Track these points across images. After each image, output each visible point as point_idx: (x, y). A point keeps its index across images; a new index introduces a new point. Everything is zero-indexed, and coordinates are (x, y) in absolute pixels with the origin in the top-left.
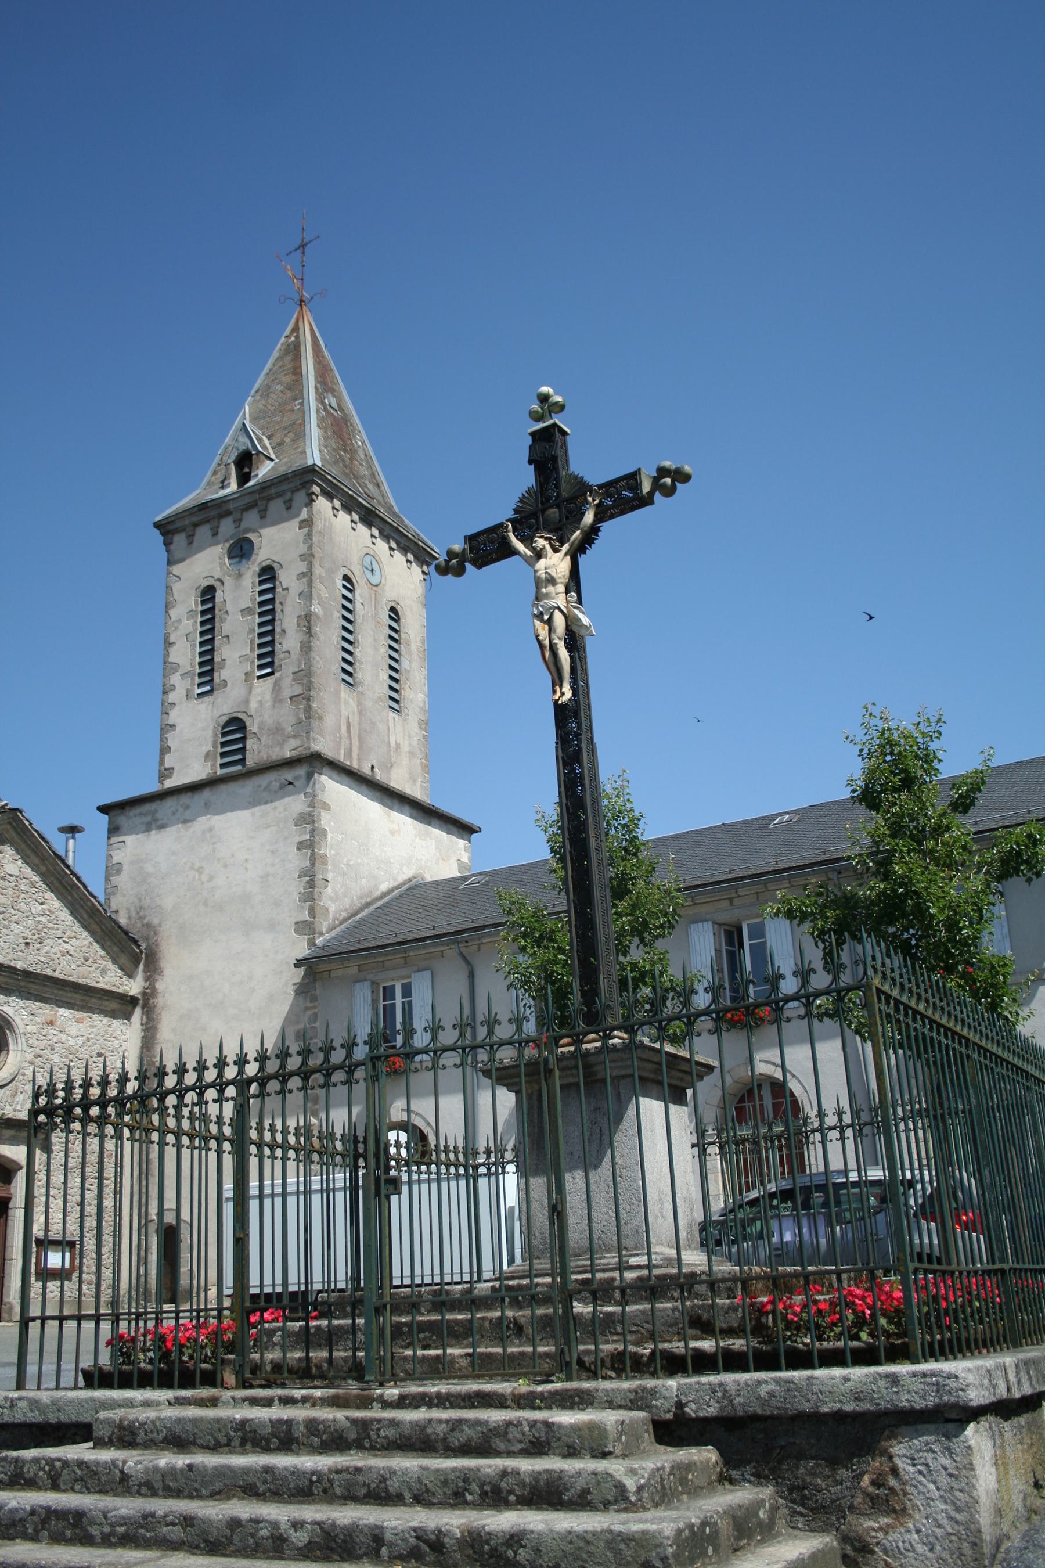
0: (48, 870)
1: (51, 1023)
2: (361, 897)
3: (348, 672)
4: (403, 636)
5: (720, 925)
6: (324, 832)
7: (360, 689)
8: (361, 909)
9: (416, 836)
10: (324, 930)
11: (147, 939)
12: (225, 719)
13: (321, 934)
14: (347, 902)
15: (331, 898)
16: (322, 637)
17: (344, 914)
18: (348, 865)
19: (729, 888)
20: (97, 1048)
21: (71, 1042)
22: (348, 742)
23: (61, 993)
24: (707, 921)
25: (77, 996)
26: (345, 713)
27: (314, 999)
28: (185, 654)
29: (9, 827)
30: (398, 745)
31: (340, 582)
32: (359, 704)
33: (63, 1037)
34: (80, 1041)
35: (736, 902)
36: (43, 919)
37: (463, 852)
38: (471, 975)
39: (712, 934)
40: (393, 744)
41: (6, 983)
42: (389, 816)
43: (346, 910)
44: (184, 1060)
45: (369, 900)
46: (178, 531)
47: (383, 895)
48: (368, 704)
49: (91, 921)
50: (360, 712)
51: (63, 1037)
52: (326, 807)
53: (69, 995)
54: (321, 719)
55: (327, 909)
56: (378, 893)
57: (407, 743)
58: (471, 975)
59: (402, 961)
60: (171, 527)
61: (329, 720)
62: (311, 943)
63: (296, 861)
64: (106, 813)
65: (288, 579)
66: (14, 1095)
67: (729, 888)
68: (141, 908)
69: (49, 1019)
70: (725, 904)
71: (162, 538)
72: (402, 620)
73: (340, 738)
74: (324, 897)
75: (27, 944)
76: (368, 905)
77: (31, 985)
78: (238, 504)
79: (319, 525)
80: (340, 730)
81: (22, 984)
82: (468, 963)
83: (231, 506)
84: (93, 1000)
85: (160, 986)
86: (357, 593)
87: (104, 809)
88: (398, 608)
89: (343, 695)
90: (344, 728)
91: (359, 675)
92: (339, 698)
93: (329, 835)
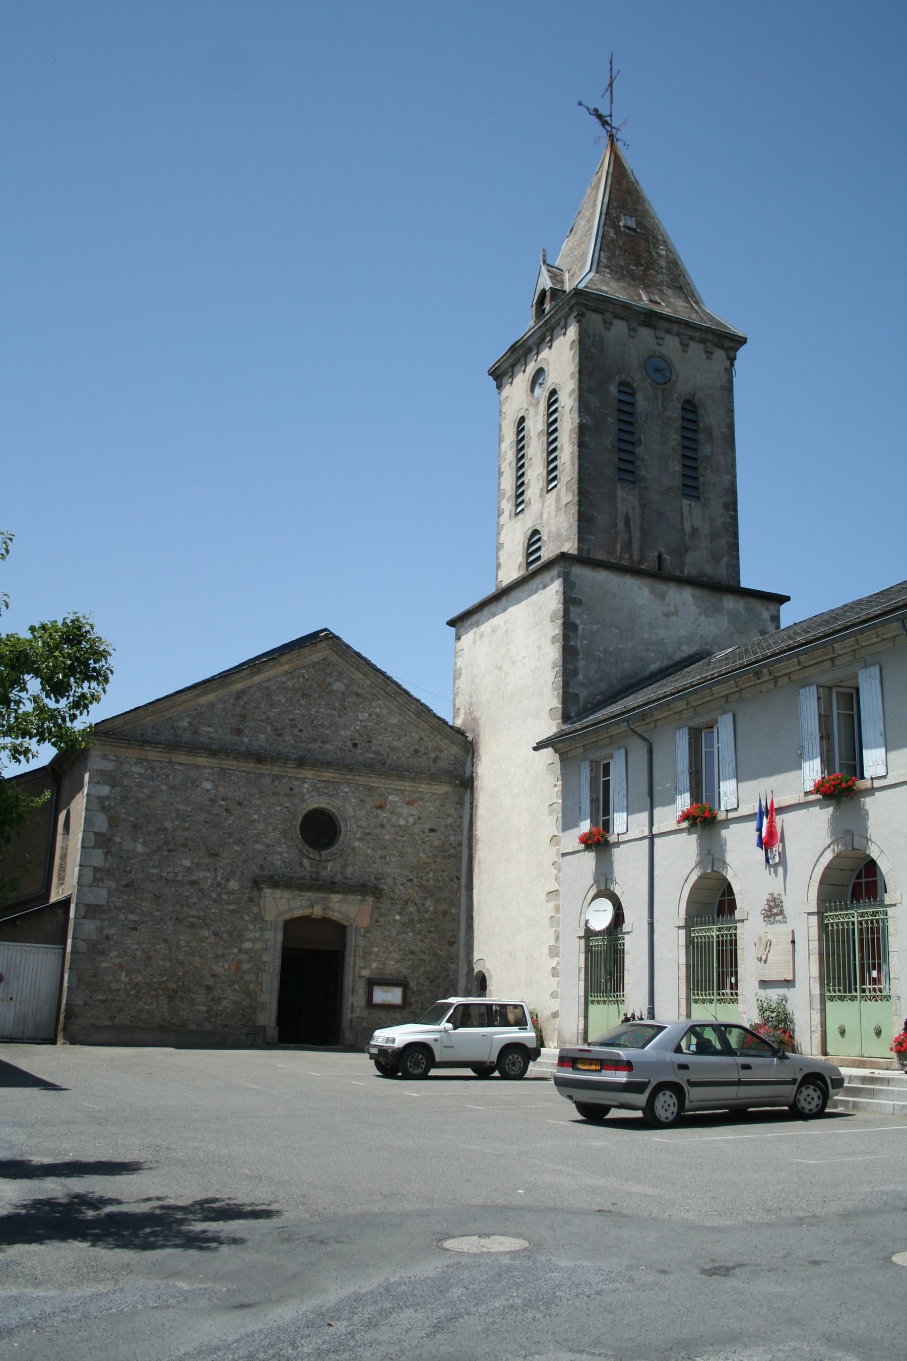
0: (372, 682)
1: (381, 807)
5: (830, 688)
7: (643, 484)
9: (700, 615)
10: (572, 715)
11: (473, 731)
12: (530, 532)
17: (599, 697)
18: (605, 651)
19: (824, 645)
23: (388, 782)
24: (812, 685)
25: (405, 783)
28: (508, 483)
29: (331, 651)
30: (695, 531)
35: (837, 662)
37: (769, 623)
38: (650, 751)
39: (816, 698)
41: (333, 778)
43: (602, 693)
45: (633, 681)
46: (501, 374)
49: (419, 720)
50: (643, 506)
53: (397, 783)
55: (577, 695)
58: (650, 751)
59: (608, 740)
60: (498, 372)
64: (454, 626)
67: (824, 645)
68: (471, 704)
69: (378, 803)
70: (828, 664)
71: (495, 383)
73: (616, 533)
75: (355, 745)
77: (357, 778)
78: (533, 340)
80: (615, 524)
81: (348, 777)
82: (645, 740)
83: (530, 343)
84: (422, 785)
87: (452, 623)
89: (619, 493)
90: (621, 525)
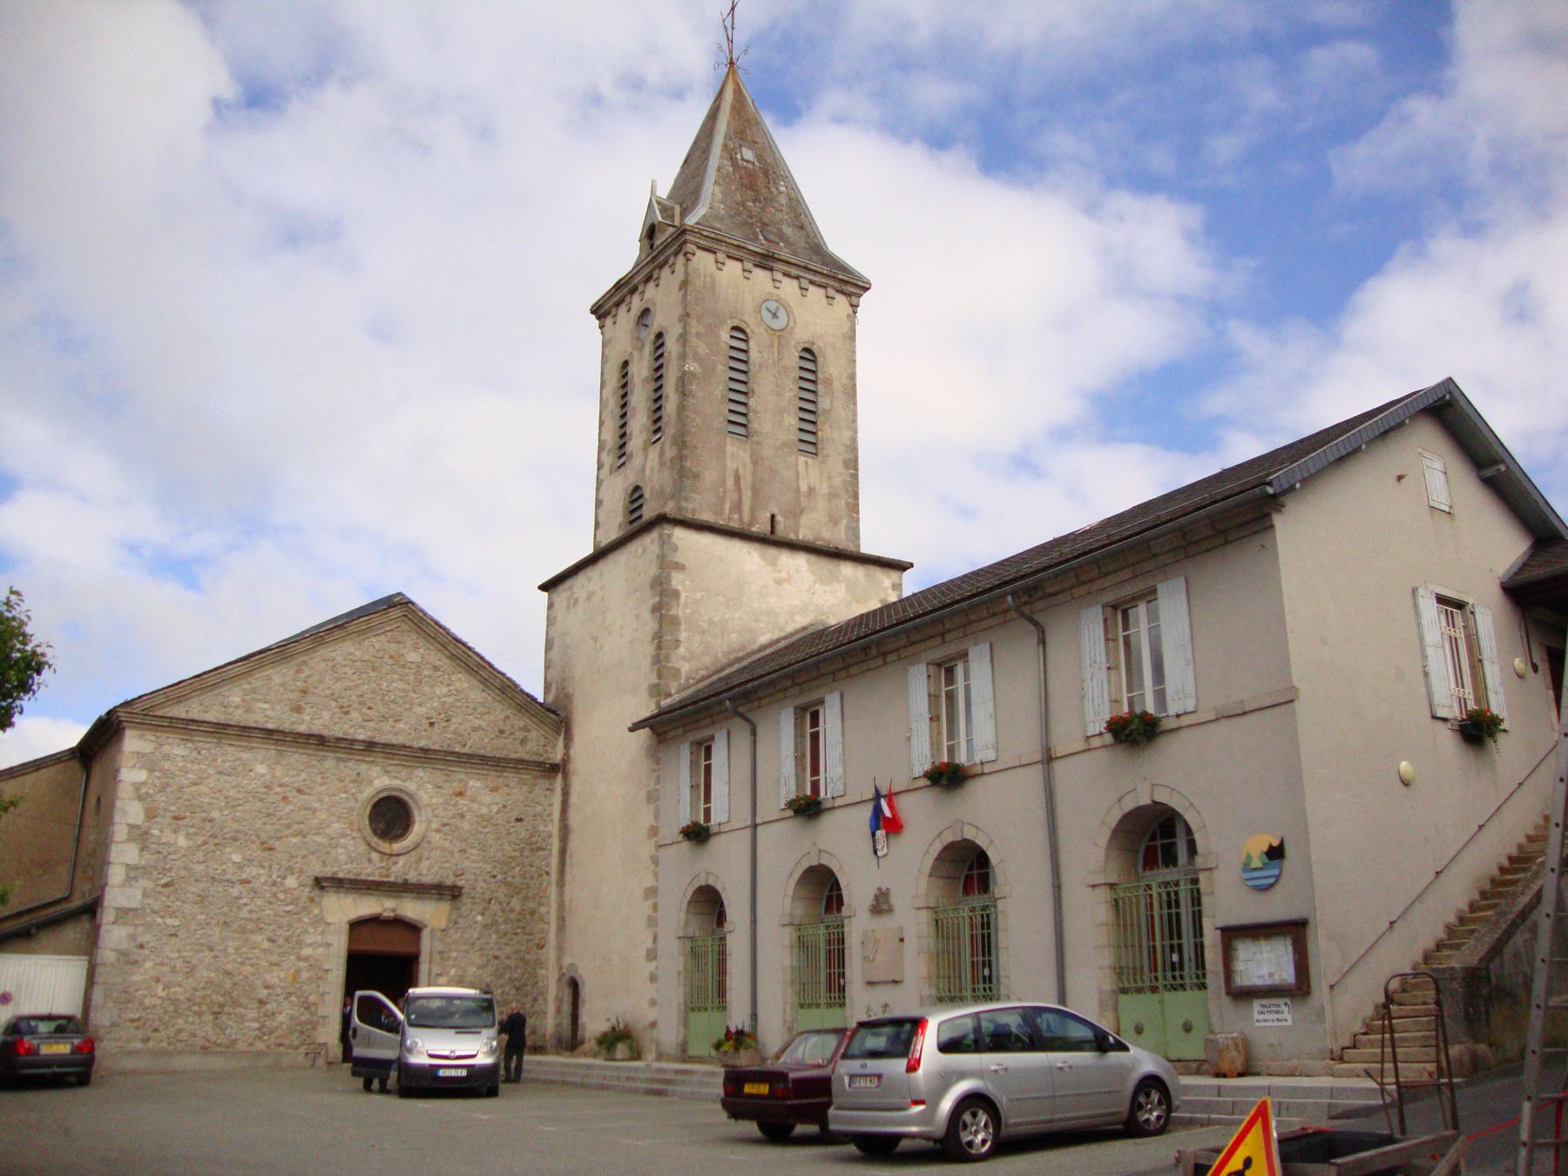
1: (460, 794)
2: (730, 653)
3: (740, 422)
4: (820, 375)
6: (676, 594)
7: (756, 439)
8: (730, 665)
13: (670, 695)
14: (708, 660)
15: (684, 658)
16: (700, 394)
17: (703, 673)
18: (710, 622)
20: (515, 814)
21: (484, 810)
22: (736, 496)
26: (731, 465)
27: (658, 762)
30: (811, 490)
31: (725, 335)
32: (753, 453)
33: (475, 806)
34: (495, 809)
36: (450, 700)
40: (804, 487)
42: (773, 563)
43: (706, 668)
44: (652, 807)
45: (741, 654)
47: (763, 648)
48: (767, 452)
50: (755, 463)
51: (475, 806)
52: (680, 567)
54: (696, 476)
56: (756, 646)
57: (825, 485)
61: (709, 476)
62: (658, 703)
63: (650, 625)
65: (672, 346)
66: (420, 860)
72: (820, 360)
74: (673, 657)
75: (432, 724)
76: (739, 660)
79: (698, 282)
85: (572, 752)
86: (752, 343)
87: (544, 587)
88: (814, 349)
89: (730, 448)
90: (730, 483)
91: (754, 426)
92: (724, 453)
93: (683, 595)
